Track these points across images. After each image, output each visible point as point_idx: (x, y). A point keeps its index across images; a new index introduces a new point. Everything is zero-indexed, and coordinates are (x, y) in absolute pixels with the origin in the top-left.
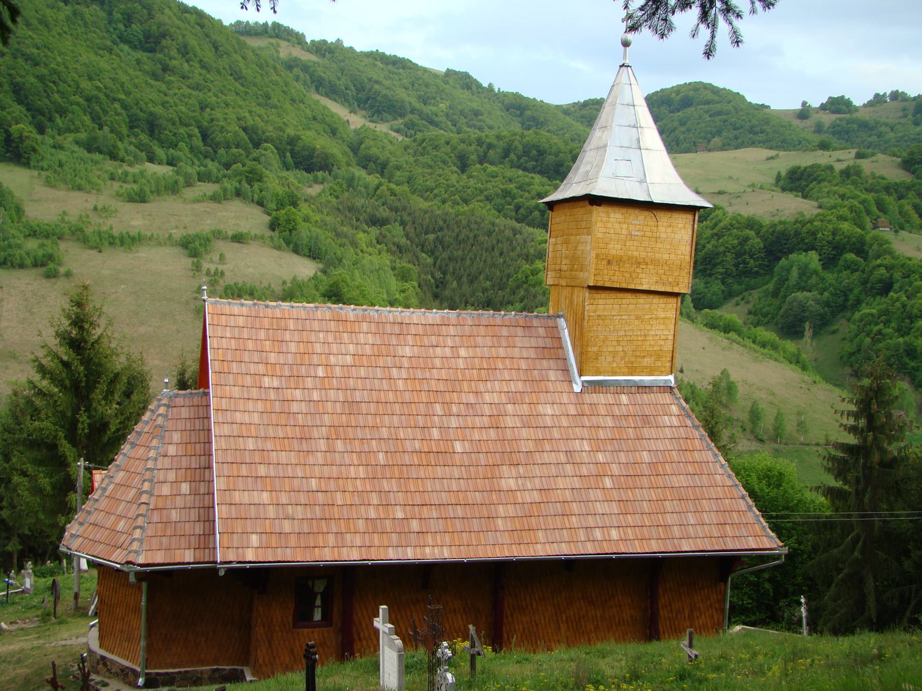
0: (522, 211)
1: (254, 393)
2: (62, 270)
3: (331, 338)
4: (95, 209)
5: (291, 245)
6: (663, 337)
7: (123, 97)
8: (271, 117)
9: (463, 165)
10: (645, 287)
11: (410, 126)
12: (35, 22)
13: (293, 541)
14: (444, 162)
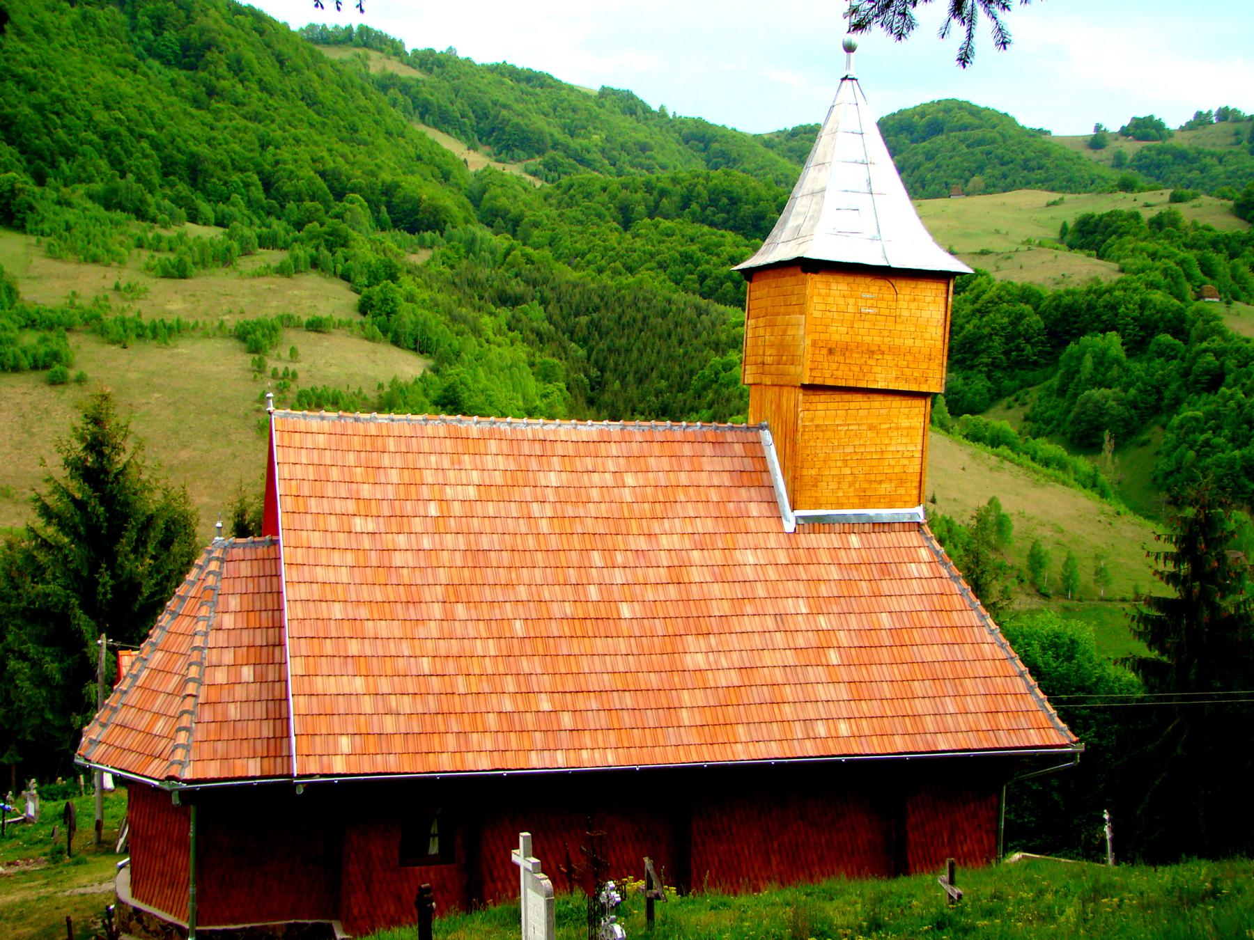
0: (709, 282)
1: (342, 540)
2: (72, 374)
4: (117, 288)
6: (906, 454)
7: (153, 132)
9: (626, 220)
10: (881, 385)
11: (552, 166)
12: (29, 30)
14: (600, 216)
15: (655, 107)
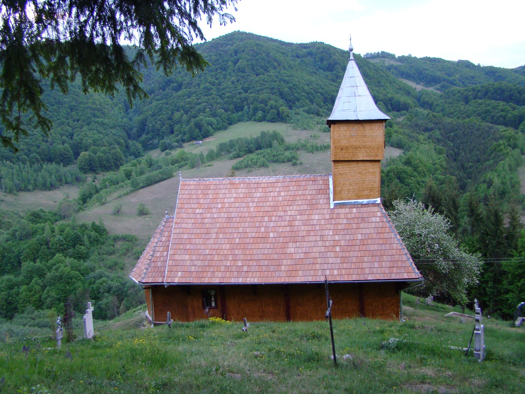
0: (495, 118)
1: (192, 216)
3: (227, 192)
4: (311, 136)
5: (390, 143)
6: (373, 181)
7: (321, 90)
8: (381, 91)
9: (467, 101)
10: (360, 159)
11: (443, 87)
12: (287, 67)
13: (194, 274)
14: (458, 101)
15: (476, 64)
